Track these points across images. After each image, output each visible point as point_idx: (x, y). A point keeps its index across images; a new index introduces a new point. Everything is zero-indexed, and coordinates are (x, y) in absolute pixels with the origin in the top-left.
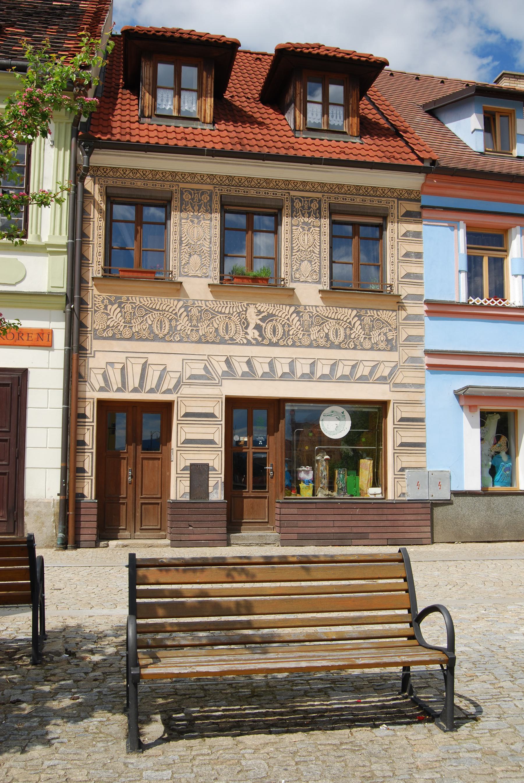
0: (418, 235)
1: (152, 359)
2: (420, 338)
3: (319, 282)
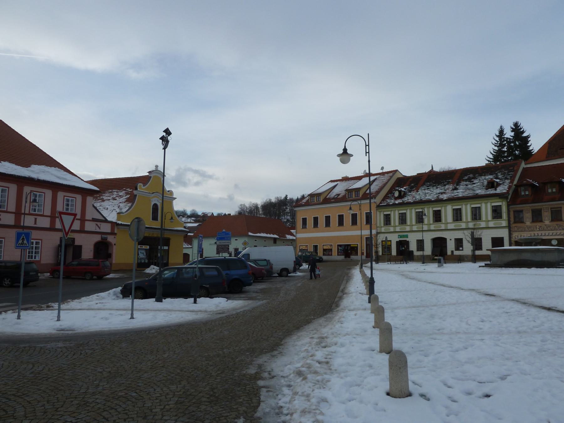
1: (522, 234)
3: (549, 220)
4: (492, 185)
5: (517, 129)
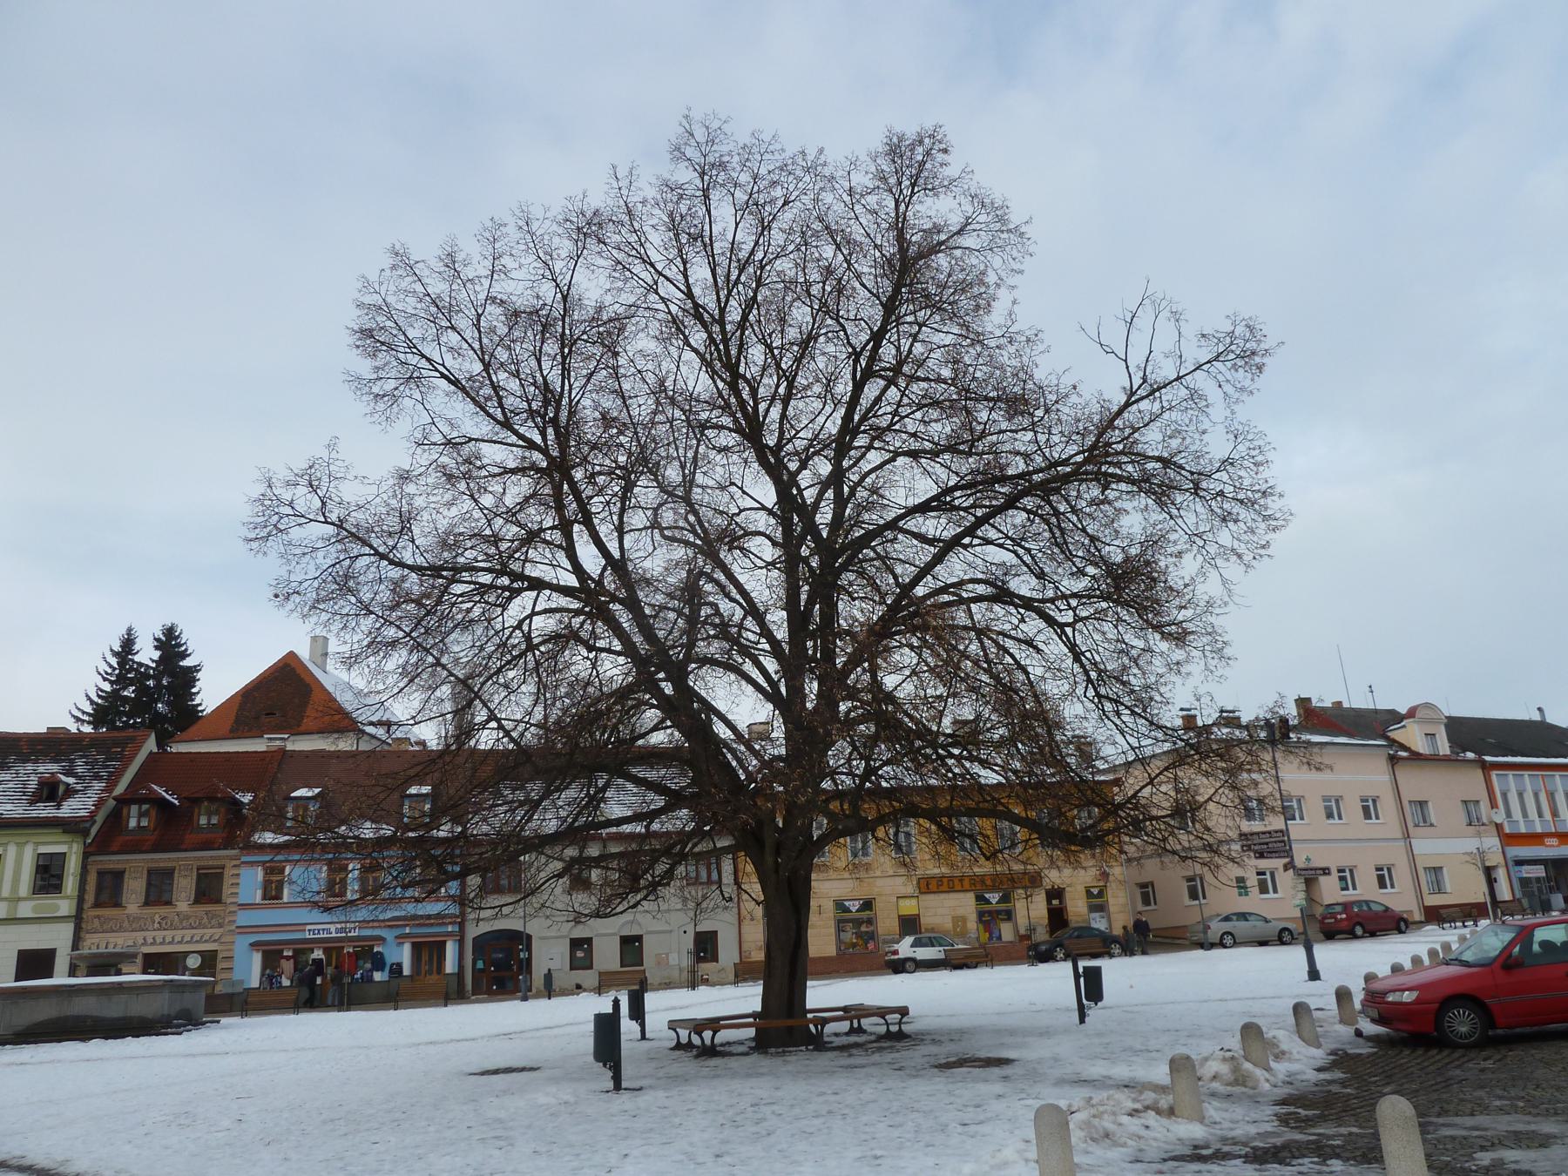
0: (238, 875)
1: (111, 940)
2: (234, 921)
4: (50, 791)
5: (170, 644)
